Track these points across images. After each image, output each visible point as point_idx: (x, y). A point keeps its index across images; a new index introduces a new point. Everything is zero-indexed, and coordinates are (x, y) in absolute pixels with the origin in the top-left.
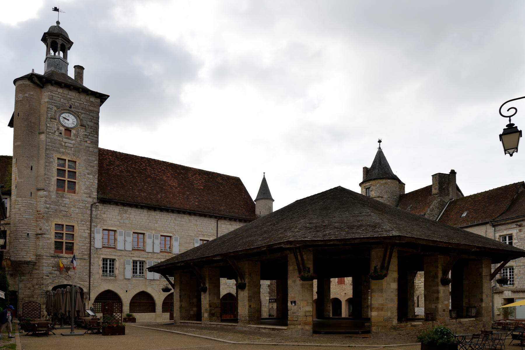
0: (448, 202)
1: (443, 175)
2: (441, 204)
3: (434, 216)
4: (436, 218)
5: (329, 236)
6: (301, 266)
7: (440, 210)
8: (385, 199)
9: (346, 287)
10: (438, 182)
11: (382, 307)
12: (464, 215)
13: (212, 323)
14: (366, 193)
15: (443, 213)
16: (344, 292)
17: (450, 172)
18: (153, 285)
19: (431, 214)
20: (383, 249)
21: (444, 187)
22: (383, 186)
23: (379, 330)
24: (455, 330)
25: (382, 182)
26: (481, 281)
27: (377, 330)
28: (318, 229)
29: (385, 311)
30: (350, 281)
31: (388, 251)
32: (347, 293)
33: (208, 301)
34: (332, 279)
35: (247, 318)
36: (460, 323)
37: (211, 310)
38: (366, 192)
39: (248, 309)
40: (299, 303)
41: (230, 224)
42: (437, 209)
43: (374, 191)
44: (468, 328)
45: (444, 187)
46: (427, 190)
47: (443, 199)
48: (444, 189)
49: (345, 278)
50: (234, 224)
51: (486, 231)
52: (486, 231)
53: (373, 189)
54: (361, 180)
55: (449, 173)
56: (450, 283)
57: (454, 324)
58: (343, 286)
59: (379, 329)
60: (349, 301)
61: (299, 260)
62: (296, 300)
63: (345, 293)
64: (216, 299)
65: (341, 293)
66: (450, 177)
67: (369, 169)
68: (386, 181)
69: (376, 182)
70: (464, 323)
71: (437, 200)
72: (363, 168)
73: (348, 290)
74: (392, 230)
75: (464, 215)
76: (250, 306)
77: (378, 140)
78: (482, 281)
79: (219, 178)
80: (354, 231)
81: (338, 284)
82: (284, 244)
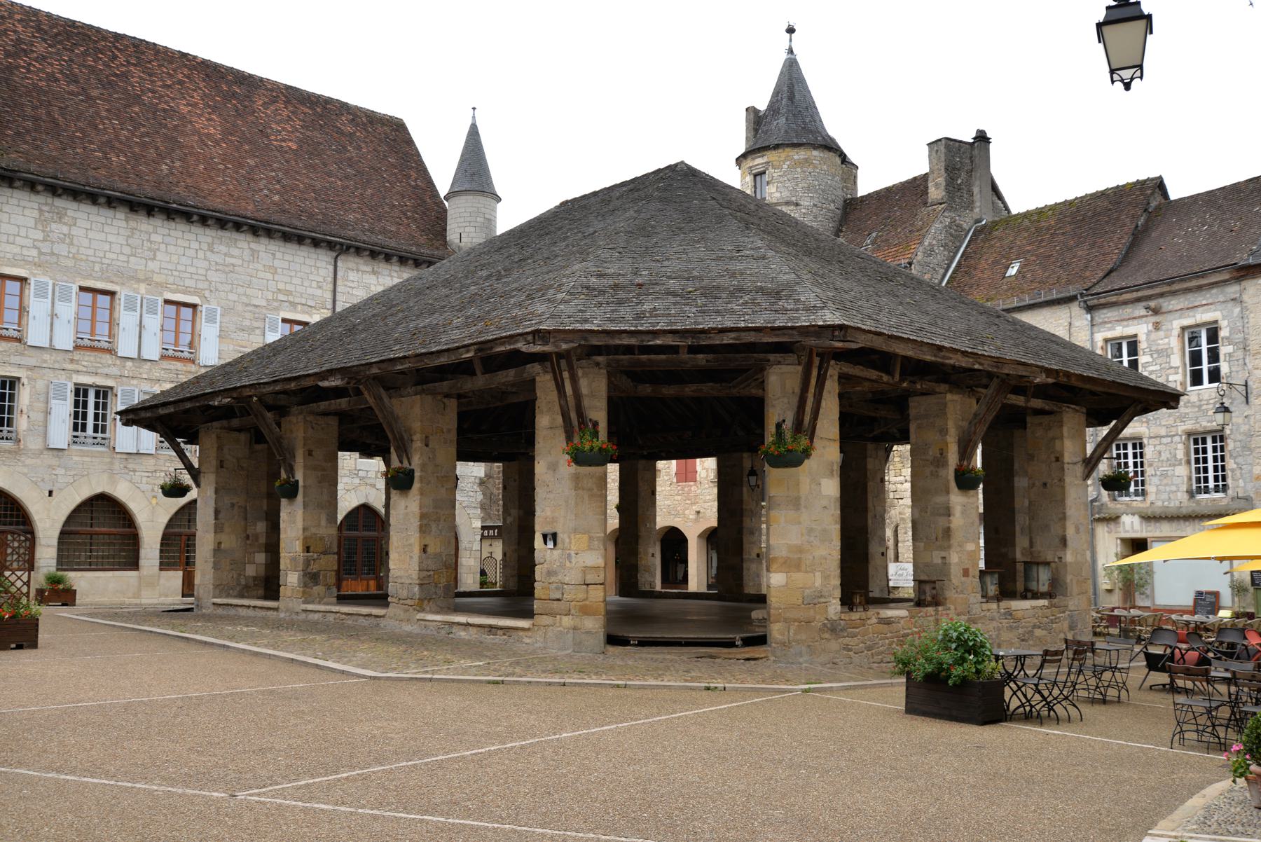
0: (970, 230)
1: (957, 144)
2: (952, 235)
5: (653, 320)
6: (573, 416)
8: (804, 211)
10: (943, 164)
16: (695, 508)
17: (974, 135)
18: (134, 471)
19: (928, 264)
20: (800, 368)
21: (959, 182)
24: (998, 636)
25: (796, 157)
27: (786, 633)
28: (622, 295)
29: (807, 572)
33: (301, 532)
36: (1009, 614)
37: (307, 562)
38: (753, 184)
41: (374, 272)
42: (942, 248)
43: (776, 185)
44: (1031, 632)
45: (959, 182)
47: (957, 218)
49: (698, 460)
50: (386, 272)
51: (1070, 324)
52: (1070, 324)
57: (992, 619)
58: (691, 486)
63: (698, 512)
65: (687, 512)
69: (780, 157)
70: (1019, 614)
71: (941, 222)
74: (822, 308)
76: (424, 549)
77: (786, 27)
82: (526, 341)
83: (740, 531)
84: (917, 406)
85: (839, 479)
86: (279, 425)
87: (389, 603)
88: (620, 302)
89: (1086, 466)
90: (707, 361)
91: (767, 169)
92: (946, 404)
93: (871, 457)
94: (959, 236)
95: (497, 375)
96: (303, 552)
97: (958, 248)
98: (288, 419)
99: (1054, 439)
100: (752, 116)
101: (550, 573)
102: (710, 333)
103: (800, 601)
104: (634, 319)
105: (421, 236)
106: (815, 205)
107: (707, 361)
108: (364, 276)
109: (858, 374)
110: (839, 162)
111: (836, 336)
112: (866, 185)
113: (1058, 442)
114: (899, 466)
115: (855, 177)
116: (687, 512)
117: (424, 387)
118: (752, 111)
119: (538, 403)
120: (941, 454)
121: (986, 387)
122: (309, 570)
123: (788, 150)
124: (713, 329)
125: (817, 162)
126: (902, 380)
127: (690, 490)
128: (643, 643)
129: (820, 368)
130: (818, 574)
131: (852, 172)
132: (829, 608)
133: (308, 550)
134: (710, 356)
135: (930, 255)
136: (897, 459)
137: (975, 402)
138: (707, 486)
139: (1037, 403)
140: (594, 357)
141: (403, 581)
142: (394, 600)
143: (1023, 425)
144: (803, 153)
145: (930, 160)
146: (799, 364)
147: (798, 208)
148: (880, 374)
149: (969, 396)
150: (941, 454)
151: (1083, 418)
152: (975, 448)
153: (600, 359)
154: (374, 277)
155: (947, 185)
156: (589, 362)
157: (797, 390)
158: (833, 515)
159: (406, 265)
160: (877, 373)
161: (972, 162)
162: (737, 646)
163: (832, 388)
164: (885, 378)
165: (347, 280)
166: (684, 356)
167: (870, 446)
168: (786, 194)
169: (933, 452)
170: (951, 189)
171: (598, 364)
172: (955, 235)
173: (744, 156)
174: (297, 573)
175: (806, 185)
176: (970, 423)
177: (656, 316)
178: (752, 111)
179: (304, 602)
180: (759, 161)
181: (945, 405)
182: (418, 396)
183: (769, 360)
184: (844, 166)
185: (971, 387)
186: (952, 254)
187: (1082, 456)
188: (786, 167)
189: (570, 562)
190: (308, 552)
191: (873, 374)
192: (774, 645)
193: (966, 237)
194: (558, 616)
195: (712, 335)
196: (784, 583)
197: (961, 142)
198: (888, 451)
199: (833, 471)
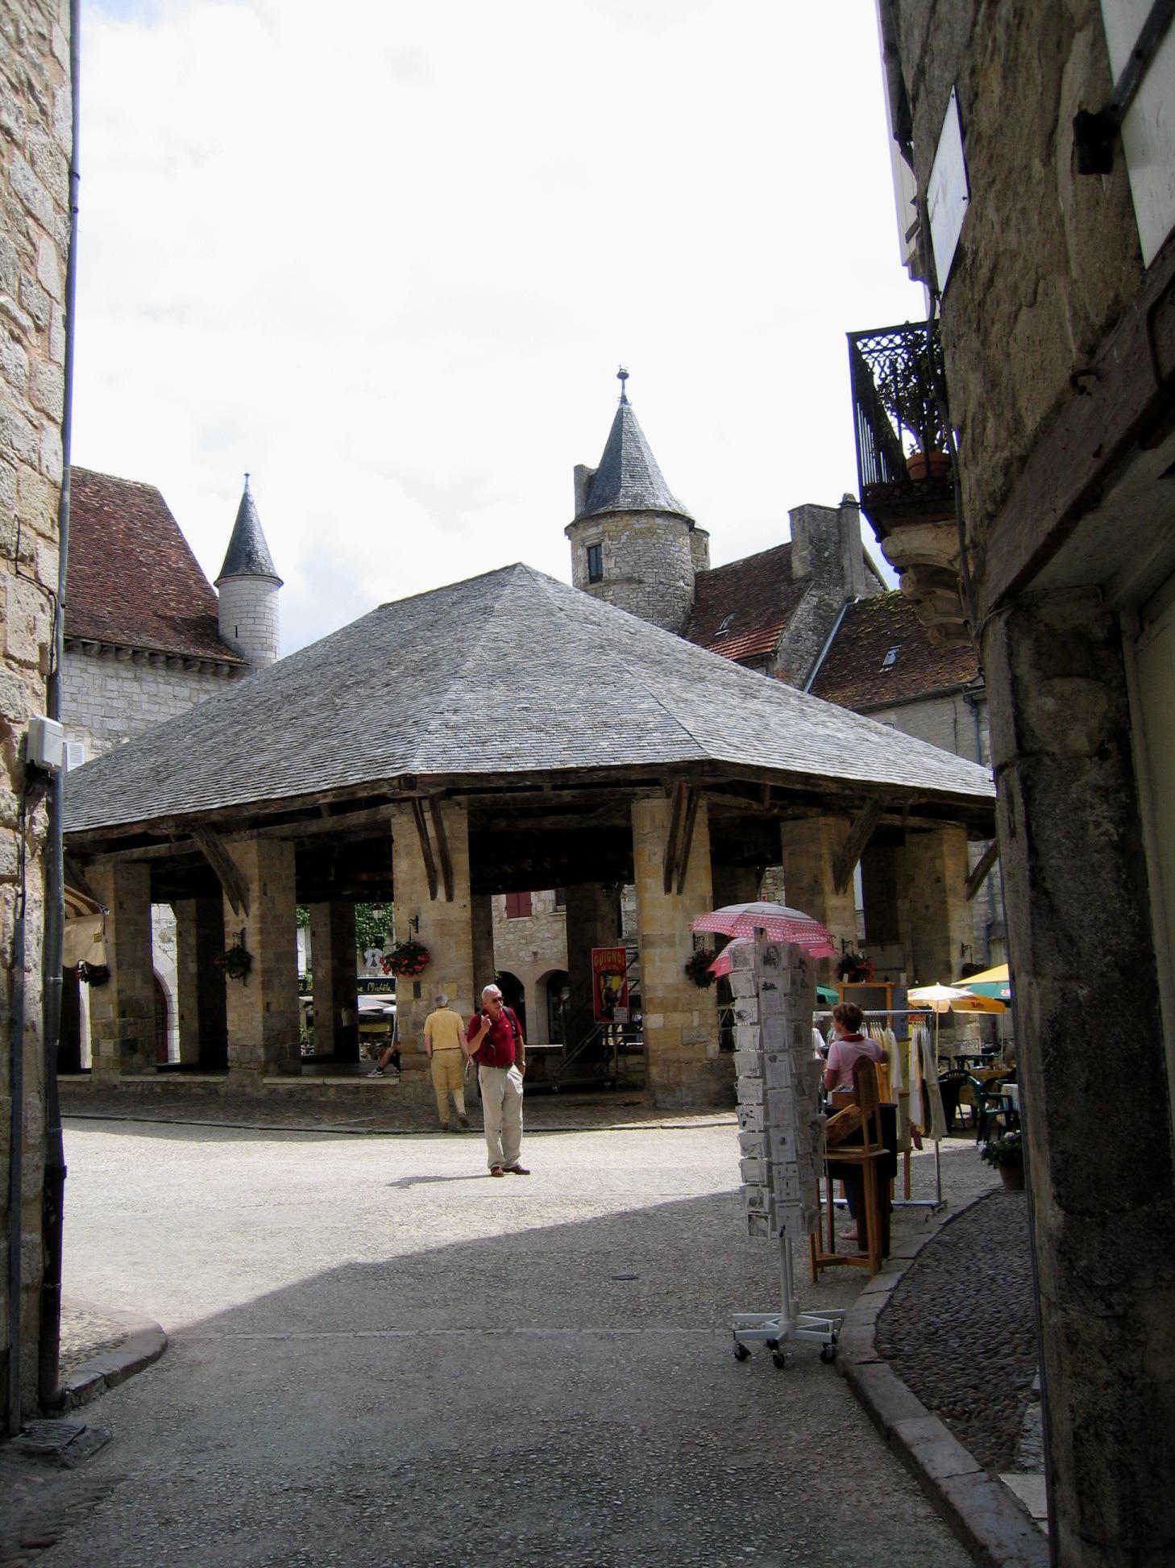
0: (841, 610)
1: (822, 511)
2: (821, 617)
3: (802, 657)
4: (808, 665)
6: (436, 859)
7: (819, 636)
8: (648, 589)
12: (890, 659)
13: (129, 1079)
14: (587, 565)
16: (532, 948)
17: (841, 501)
19: (795, 651)
21: (826, 554)
22: (640, 541)
25: (637, 526)
26: (944, 902)
30: (547, 902)
32: (540, 951)
33: (115, 995)
34: (494, 898)
35: (261, 1052)
37: (123, 1028)
38: (587, 558)
39: (264, 1017)
41: (137, 679)
42: (810, 633)
45: (826, 554)
46: (774, 562)
47: (826, 597)
48: (827, 562)
49: (533, 893)
50: (150, 678)
51: (955, 721)
52: (955, 721)
54: (570, 517)
55: (839, 507)
56: (225, 977)
60: (552, 982)
63: (535, 954)
64: (139, 983)
65: (522, 954)
68: (651, 521)
69: (617, 526)
71: (808, 603)
73: (544, 940)
75: (890, 659)
76: (267, 1006)
77: (618, 372)
78: (946, 902)
79: (87, 490)
81: (508, 918)
82: (391, 786)
84: (788, 829)
86: (83, 873)
87: (229, 1068)
89: (970, 885)
91: (603, 540)
95: (346, 817)
96: (119, 1017)
97: (828, 632)
98: (91, 868)
99: (933, 859)
105: (189, 631)
107: (573, 797)
108: (125, 684)
110: (687, 530)
111: (706, 771)
112: (719, 557)
113: (938, 862)
115: (706, 545)
117: (261, 830)
118: (579, 470)
119: (395, 847)
120: (816, 882)
121: (860, 808)
122: (125, 1038)
123: (627, 518)
126: (772, 806)
127: (525, 927)
129: (690, 801)
130: (696, 1013)
133: (122, 1014)
135: (797, 641)
136: (769, 881)
137: (848, 825)
138: (545, 921)
139: (914, 821)
140: (455, 797)
141: (245, 1043)
142: (235, 1064)
143: (902, 843)
144: (645, 521)
147: (641, 586)
150: (816, 882)
151: (963, 834)
152: (852, 868)
153: (461, 798)
154: (136, 685)
157: (668, 824)
159: (173, 670)
160: (747, 801)
161: (840, 531)
163: (702, 817)
164: (755, 805)
165: (106, 690)
166: (548, 792)
168: (626, 570)
169: (806, 881)
171: (459, 804)
172: (824, 615)
173: (573, 525)
174: (112, 1041)
175: (649, 559)
178: (579, 470)
179: (124, 1073)
180: (593, 531)
182: (254, 841)
183: (636, 794)
187: (964, 875)
190: (124, 1017)
191: (743, 801)
193: (837, 618)
196: (661, 1024)
198: (760, 876)
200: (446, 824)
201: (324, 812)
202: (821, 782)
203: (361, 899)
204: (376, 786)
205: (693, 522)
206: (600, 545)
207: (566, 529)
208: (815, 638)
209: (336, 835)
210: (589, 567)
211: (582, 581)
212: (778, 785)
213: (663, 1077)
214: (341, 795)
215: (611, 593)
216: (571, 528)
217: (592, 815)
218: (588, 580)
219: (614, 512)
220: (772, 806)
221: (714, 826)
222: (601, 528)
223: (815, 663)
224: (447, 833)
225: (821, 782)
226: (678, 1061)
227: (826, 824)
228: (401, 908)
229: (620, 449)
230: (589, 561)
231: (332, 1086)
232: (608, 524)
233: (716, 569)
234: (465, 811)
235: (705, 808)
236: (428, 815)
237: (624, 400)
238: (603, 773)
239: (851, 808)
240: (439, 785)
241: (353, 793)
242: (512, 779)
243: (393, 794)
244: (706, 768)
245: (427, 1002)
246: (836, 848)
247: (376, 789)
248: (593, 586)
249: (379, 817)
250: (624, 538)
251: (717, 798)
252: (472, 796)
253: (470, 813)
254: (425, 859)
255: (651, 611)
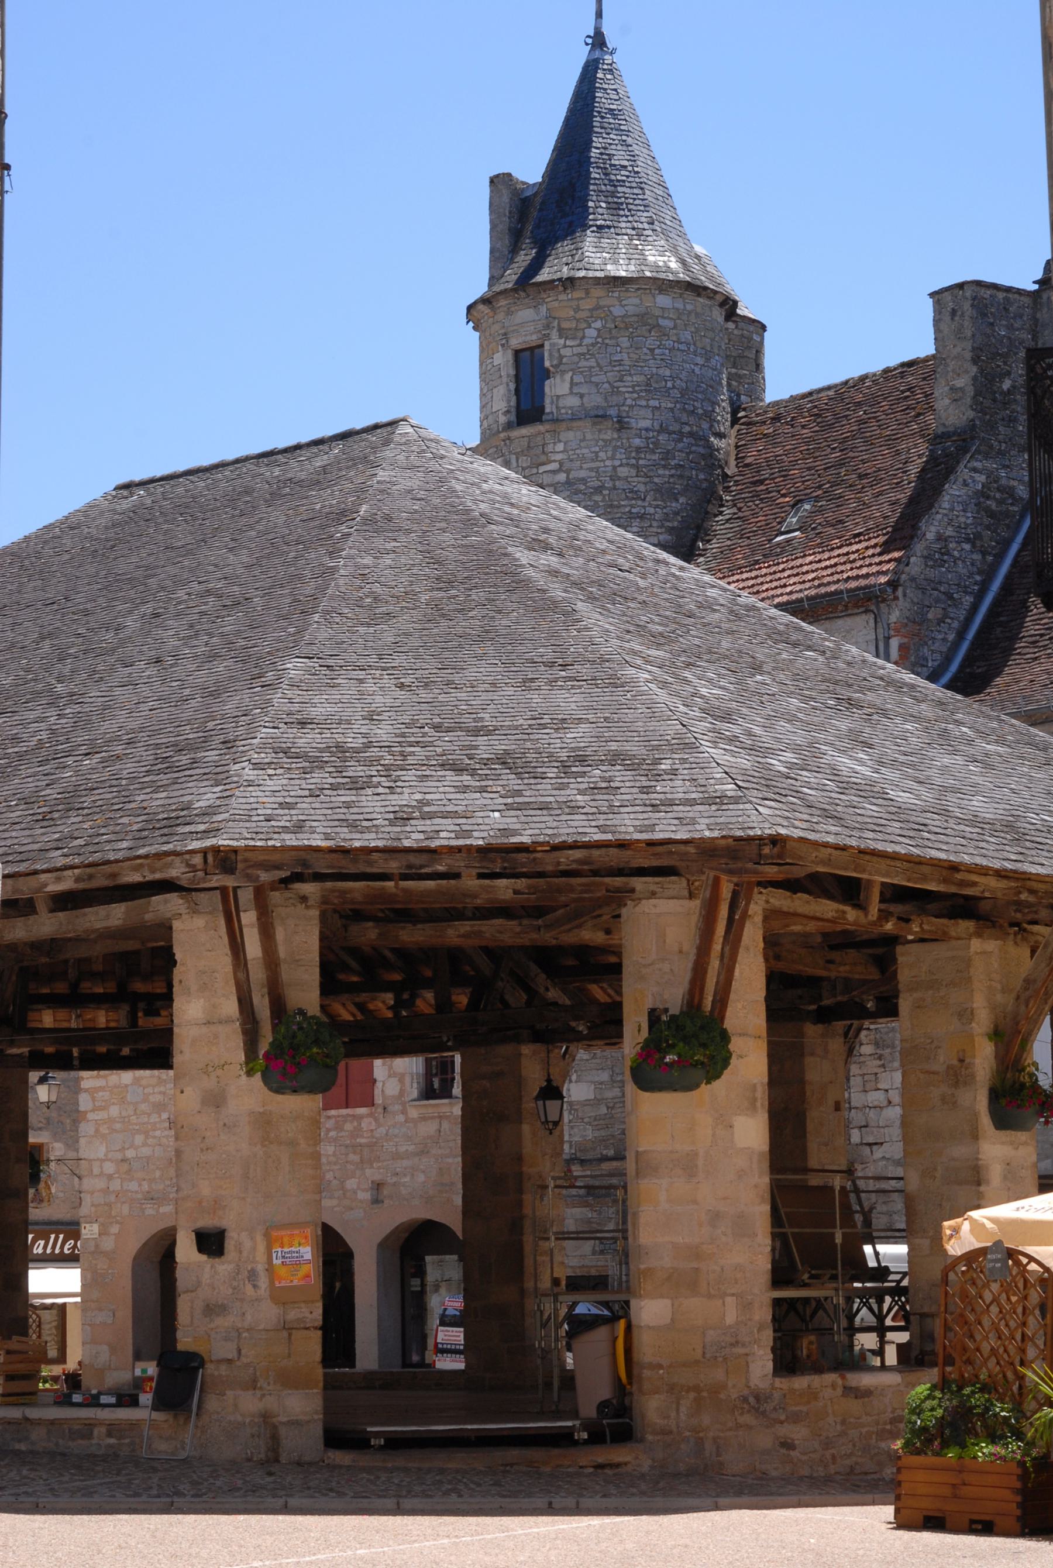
1: (1001, 295)
2: (991, 514)
3: (950, 596)
4: (962, 614)
5: (428, 825)
7: (984, 554)
8: (637, 442)
9: (382, 1130)
10: (969, 345)
11: (695, 1265)
14: (512, 386)
15: (1008, 577)
16: (373, 1174)
17: (1039, 275)
19: (935, 584)
20: (696, 904)
21: (1007, 385)
23: (683, 1417)
25: (617, 311)
27: (673, 1414)
28: (356, 770)
29: (710, 1296)
30: (408, 1080)
31: (721, 916)
38: (512, 372)
40: (247, 1244)
42: (967, 547)
43: (568, 376)
45: (1007, 385)
49: (378, 1063)
53: (561, 357)
54: (480, 287)
55: (1036, 287)
58: (360, 1118)
59: (683, 1409)
61: (249, 956)
62: (227, 1220)
63: (378, 1186)
66: (1038, 315)
67: (528, 193)
69: (577, 309)
72: (493, 181)
73: (397, 1156)
74: (736, 800)
80: (545, 791)
82: (188, 865)
83: (516, 1226)
85: (766, 1115)
88: (356, 785)
90: (516, 892)
91: (547, 337)
92: (970, 960)
93: (812, 1054)
94: (1007, 514)
95: (85, 915)
97: (1007, 543)
100: (506, 199)
101: (212, 1310)
102: (535, 851)
103: (699, 1351)
104: (392, 823)
106: (662, 430)
109: (800, 910)
110: (721, 319)
111: (766, 856)
114: (873, 1065)
115: (759, 352)
116: (351, 1184)
118: (500, 182)
120: (962, 1061)
124: (542, 844)
125: (671, 324)
126: (885, 916)
127: (358, 1129)
128: (395, 1444)
131: (750, 339)
132: (752, 1366)
134: (521, 883)
136: (867, 1049)
137: (1028, 952)
145: (937, 330)
146: (691, 896)
148: (842, 907)
149: (1016, 943)
150: (962, 1061)
153: (308, 888)
155: (977, 394)
156: (288, 894)
158: (756, 1186)
162: (576, 1443)
163: (753, 935)
164: (852, 914)
166: (470, 882)
167: (812, 1030)
168: (594, 400)
169: (944, 1059)
170: (987, 403)
173: (485, 300)
176: (1018, 998)
177: (431, 816)
178: (500, 182)
181: (968, 962)
183: (633, 891)
184: (731, 325)
185: (1017, 924)
186: (990, 558)
188: (595, 333)
189: (255, 1286)
191: (827, 908)
192: (650, 1437)
194: (230, 1394)
195: (538, 855)
197: (1009, 290)
199: (755, 1100)
200: (280, 934)
201: (41, 906)
202: (974, 878)
203: (41, 1061)
204: (159, 864)
205: (735, 303)
206: (542, 346)
207: (470, 308)
208: (977, 557)
209: (52, 945)
210: (517, 391)
211: (503, 419)
212: (895, 882)
213: (668, 1417)
214: (91, 877)
215: (560, 447)
216: (481, 307)
217: (540, 922)
218: (513, 417)
219: (571, 280)
220: (885, 916)
221: (772, 944)
222: (543, 309)
223: (974, 608)
224: (282, 952)
225: (974, 878)
226: (697, 1389)
227: (984, 953)
228: (188, 1090)
229: (588, 145)
230: (517, 378)
231: (39, 1422)
232: (559, 303)
233: (776, 404)
234: (315, 913)
235: (758, 919)
236: (249, 918)
237: (598, 41)
238: (577, 854)
239: (1035, 922)
240: (278, 867)
241: (114, 876)
242: (413, 859)
243: (192, 881)
244: (766, 850)
245: (232, 1266)
246: (999, 998)
247: (160, 870)
248: (525, 431)
249: (148, 917)
250: (591, 333)
251: (780, 900)
252: (329, 884)
253: (323, 916)
254: (240, 1000)
255: (642, 488)
